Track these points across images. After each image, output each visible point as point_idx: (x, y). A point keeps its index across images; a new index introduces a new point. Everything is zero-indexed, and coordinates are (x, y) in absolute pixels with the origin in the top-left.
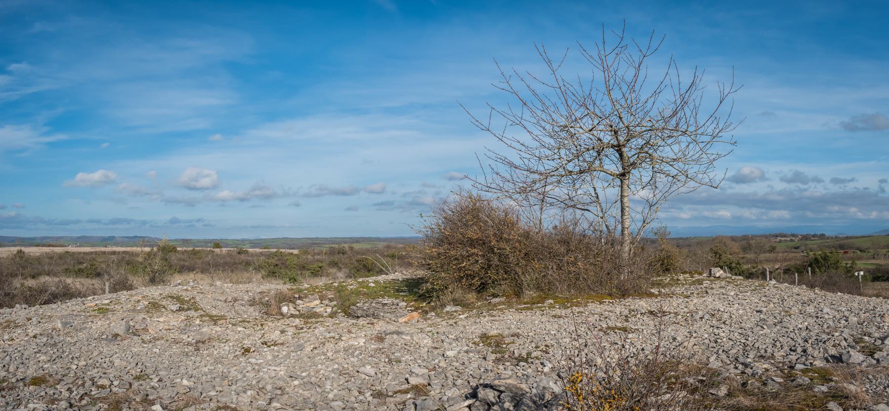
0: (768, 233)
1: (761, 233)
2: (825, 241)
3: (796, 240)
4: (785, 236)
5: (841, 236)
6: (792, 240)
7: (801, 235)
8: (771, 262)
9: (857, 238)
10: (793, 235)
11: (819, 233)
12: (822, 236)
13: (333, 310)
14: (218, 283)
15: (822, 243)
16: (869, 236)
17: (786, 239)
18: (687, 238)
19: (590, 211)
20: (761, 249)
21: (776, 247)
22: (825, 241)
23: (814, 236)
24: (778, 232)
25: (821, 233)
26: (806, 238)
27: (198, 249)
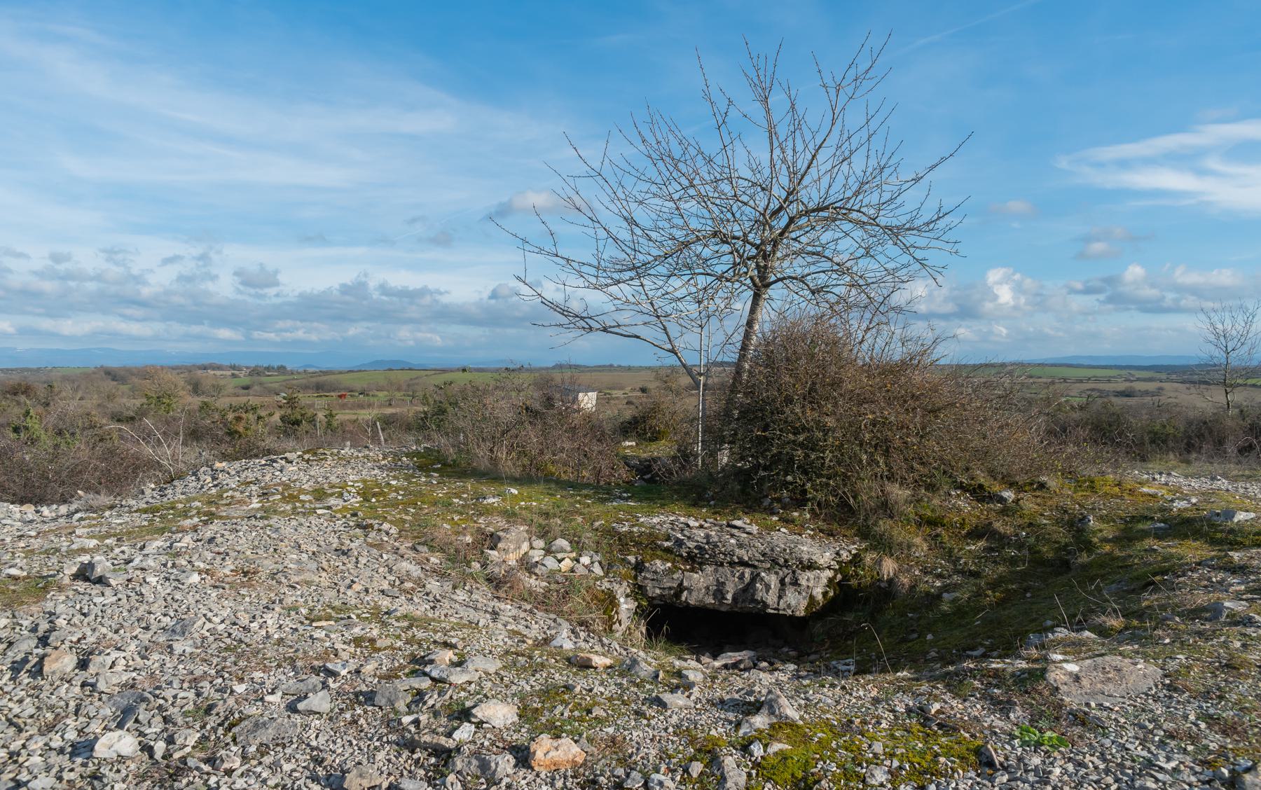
0: (188, 363)
1: (176, 362)
2: (291, 377)
3: (242, 375)
4: (219, 368)
5: (311, 370)
6: (234, 376)
7: (247, 368)
8: (541, 487)
9: (341, 373)
10: (233, 367)
11: (276, 364)
12: (281, 370)
13: (766, 315)
14: (1031, 329)
15: (284, 381)
16: (410, 369)
17: (224, 373)
18: (39, 369)
19: (638, 337)
20: (344, 393)
21: (224, 386)
22: (291, 377)
23: (268, 369)
24: (206, 362)
25: (279, 364)
26: (255, 372)
27: (630, 444)
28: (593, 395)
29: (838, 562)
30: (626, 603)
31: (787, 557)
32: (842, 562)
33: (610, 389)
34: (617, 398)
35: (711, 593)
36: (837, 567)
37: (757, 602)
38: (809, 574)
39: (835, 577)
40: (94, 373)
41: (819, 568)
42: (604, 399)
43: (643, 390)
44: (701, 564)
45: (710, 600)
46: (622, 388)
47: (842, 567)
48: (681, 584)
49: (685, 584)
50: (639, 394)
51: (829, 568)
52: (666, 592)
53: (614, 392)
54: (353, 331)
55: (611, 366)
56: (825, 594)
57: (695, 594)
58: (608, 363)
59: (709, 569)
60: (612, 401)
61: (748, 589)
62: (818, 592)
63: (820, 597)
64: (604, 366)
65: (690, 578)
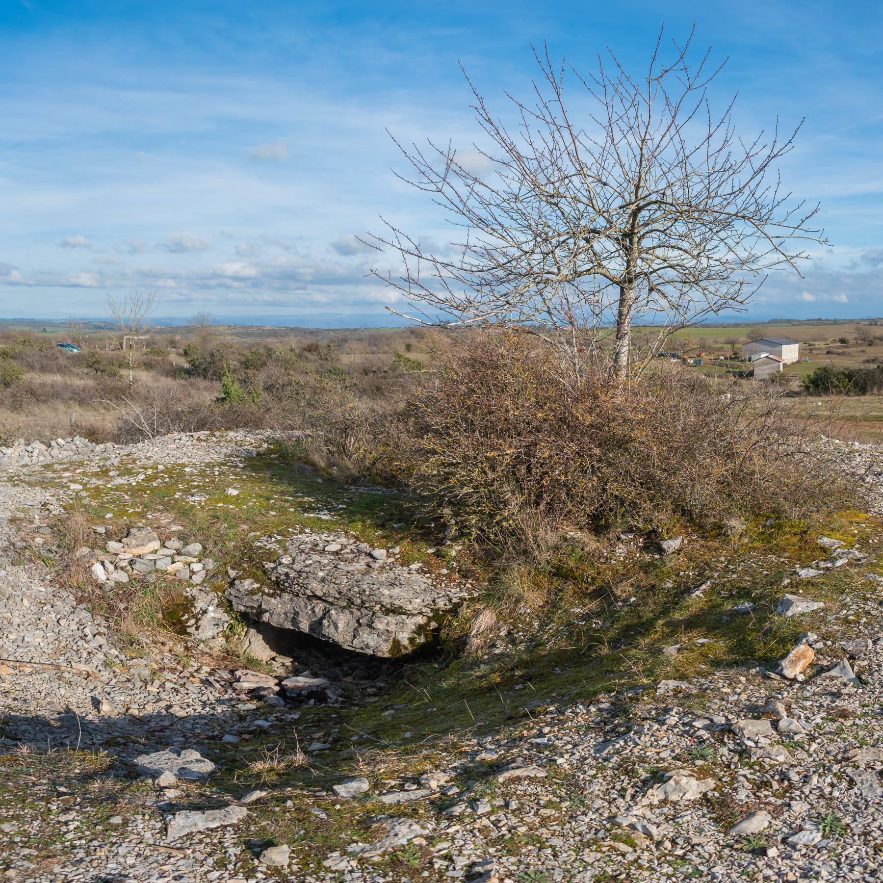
28: (796, 347)
29: (432, 610)
30: (214, 612)
31: (365, 598)
32: (438, 610)
33: (815, 340)
34: (818, 349)
35: (289, 619)
36: (431, 614)
37: (324, 636)
38: (391, 619)
39: (427, 624)
40: (403, 332)
41: (404, 614)
42: (808, 350)
43: (843, 341)
44: (283, 591)
45: (288, 626)
46: (825, 339)
47: (438, 616)
48: (260, 606)
49: (263, 607)
50: (839, 344)
51: (421, 613)
52: (249, 610)
53: (817, 343)
54: (227, 338)
55: (820, 320)
56: (412, 640)
57: (275, 617)
58: (817, 317)
59: (286, 597)
60: (815, 352)
61: (317, 625)
62: (404, 637)
63: (406, 642)
64: (814, 320)
65: (269, 603)
